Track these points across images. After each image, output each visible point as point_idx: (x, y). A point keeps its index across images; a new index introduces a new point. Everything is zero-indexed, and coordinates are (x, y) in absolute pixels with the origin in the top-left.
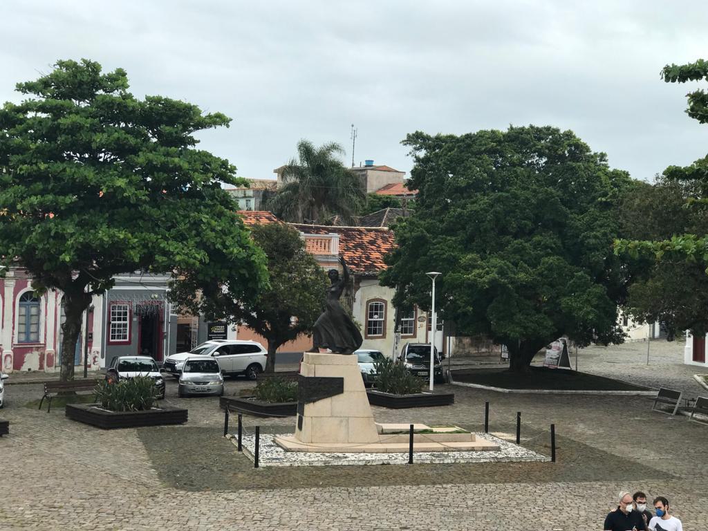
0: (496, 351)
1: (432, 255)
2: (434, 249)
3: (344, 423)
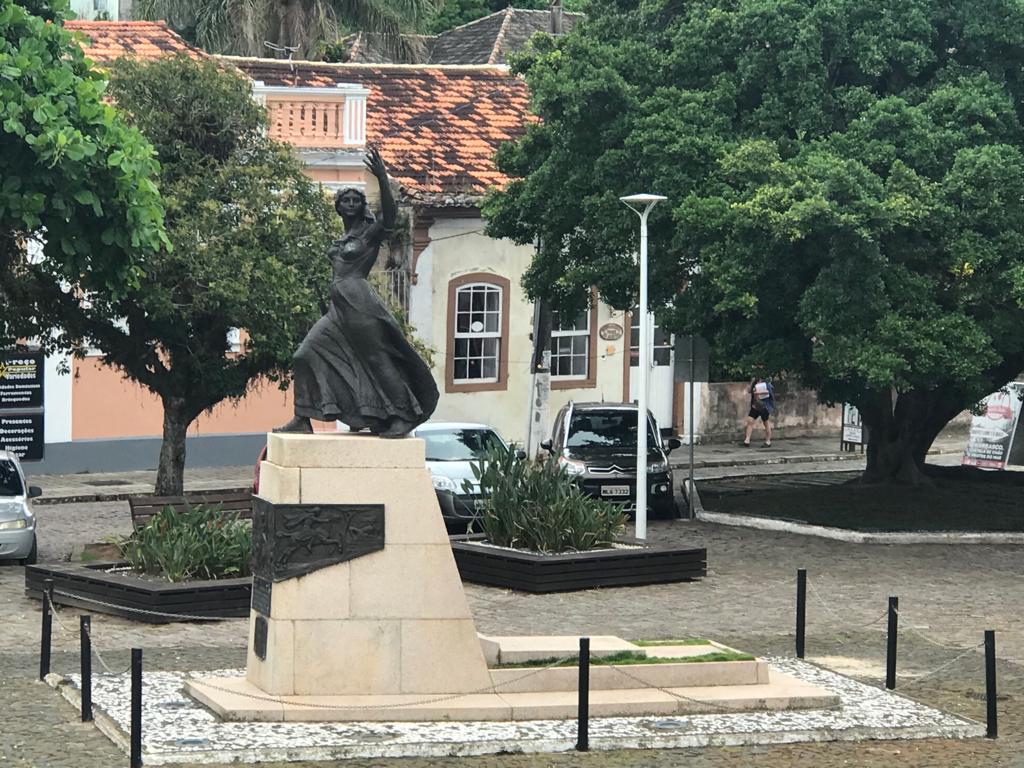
1: (639, 146)
3: (386, 639)
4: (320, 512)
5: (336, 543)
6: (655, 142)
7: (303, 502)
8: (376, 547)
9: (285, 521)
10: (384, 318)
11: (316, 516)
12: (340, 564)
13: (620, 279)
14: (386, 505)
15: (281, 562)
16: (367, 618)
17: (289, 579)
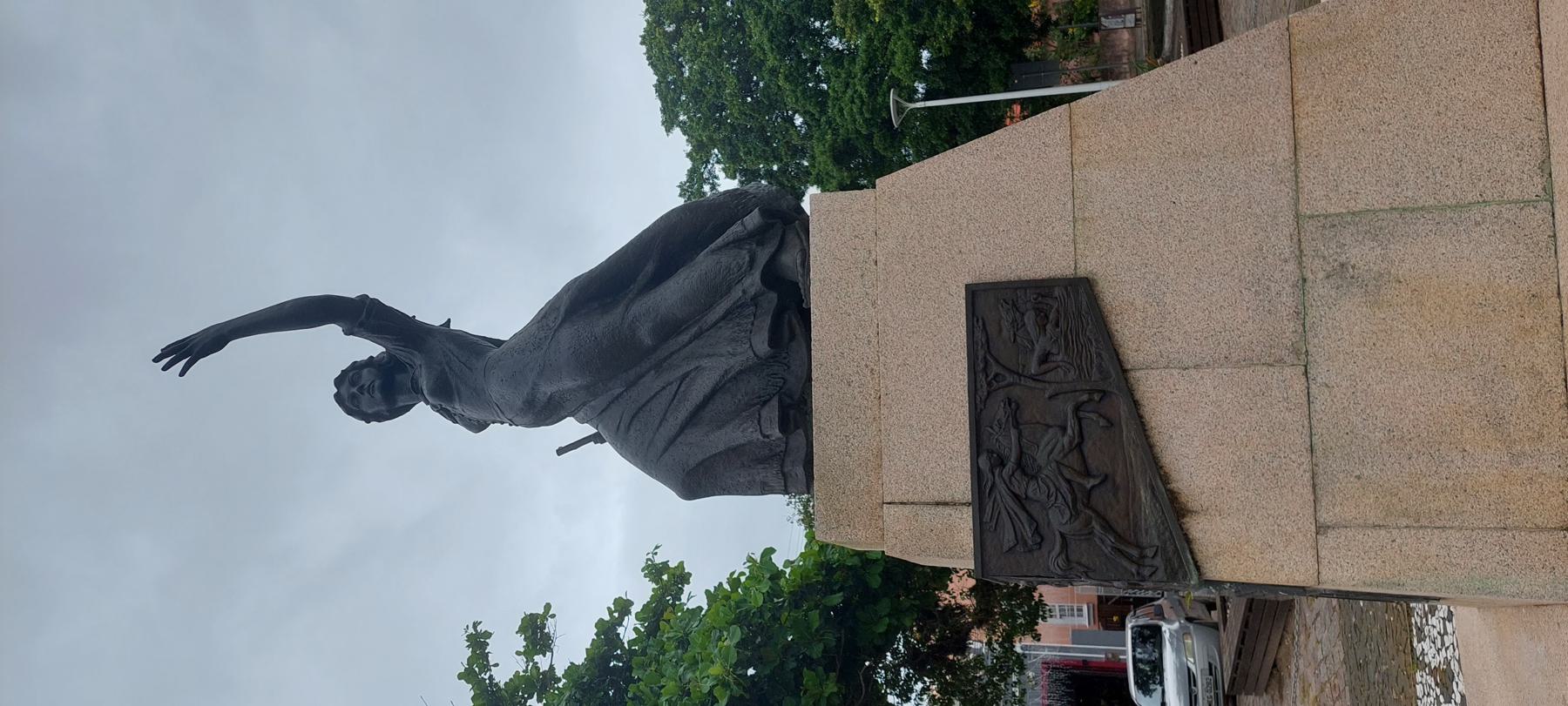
0: (1126, 44)
1: (865, 120)
2: (855, 121)
3: (1362, 255)
4: (990, 452)
5: (1077, 409)
6: (861, 109)
7: (968, 497)
8: (1084, 299)
9: (1020, 548)
10: (562, 310)
11: (1002, 464)
12: (1138, 396)
13: (971, 127)
14: (969, 281)
15: (1139, 562)
16: (1301, 314)
17: (1188, 541)
